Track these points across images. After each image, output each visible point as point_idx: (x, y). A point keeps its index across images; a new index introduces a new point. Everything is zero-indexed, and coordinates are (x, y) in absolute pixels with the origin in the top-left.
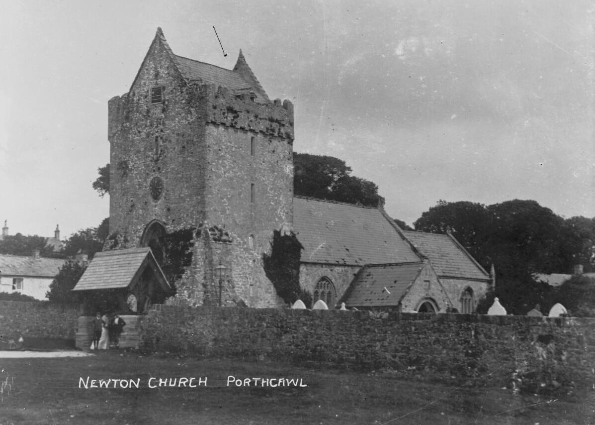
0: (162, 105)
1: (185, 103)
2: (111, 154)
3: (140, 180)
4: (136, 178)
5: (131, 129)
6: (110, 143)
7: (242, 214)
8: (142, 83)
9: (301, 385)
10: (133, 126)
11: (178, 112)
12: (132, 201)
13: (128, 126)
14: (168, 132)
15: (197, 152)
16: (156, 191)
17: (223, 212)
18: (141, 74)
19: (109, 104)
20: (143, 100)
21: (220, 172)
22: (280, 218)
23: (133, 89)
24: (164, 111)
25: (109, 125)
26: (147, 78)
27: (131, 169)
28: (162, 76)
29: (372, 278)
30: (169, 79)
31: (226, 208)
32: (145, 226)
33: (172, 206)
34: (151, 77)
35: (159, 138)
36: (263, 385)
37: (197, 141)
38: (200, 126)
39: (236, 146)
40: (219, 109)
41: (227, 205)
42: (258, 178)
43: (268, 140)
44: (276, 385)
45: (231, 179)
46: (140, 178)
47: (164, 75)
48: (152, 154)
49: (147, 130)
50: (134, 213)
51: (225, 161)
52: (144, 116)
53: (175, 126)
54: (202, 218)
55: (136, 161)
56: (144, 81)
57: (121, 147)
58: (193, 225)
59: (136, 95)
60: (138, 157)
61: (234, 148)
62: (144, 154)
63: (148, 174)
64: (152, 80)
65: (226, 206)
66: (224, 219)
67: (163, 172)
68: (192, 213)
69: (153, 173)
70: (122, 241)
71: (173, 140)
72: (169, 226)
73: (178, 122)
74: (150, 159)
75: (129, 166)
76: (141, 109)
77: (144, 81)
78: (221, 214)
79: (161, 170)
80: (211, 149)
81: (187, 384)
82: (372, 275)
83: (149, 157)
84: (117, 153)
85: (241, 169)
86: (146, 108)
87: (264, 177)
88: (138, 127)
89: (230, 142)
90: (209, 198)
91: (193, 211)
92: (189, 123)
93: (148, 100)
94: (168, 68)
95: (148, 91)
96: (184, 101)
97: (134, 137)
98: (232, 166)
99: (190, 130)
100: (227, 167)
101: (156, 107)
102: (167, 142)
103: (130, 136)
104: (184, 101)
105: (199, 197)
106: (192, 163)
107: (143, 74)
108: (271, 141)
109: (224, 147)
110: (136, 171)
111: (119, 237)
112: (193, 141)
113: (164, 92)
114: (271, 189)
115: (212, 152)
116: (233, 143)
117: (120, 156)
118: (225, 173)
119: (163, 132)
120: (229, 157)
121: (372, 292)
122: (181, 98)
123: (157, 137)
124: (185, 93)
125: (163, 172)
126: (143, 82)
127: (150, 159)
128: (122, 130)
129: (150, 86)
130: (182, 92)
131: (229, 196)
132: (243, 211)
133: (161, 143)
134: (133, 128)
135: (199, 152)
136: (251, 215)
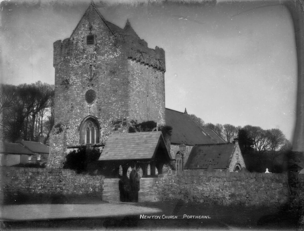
0: (95, 46)
1: (112, 45)
2: (56, 75)
3: (78, 92)
4: (75, 90)
5: (71, 60)
6: (55, 69)
7: (143, 113)
8: (79, 33)
9: (209, 218)
10: (72, 58)
11: (106, 51)
12: (72, 104)
13: (69, 58)
14: (99, 62)
15: (121, 75)
16: (90, 97)
17: (136, 112)
18: (78, 27)
19: (54, 45)
20: (80, 43)
21: (134, 88)
22: (160, 117)
23: (73, 36)
24: (96, 50)
25: (54, 58)
26: (83, 30)
27: (71, 85)
28: (95, 29)
29: (203, 152)
30: (99, 31)
31: (137, 109)
32: (82, 120)
33: (103, 107)
34: (86, 29)
35: (93, 66)
36: (140, 218)
37: (121, 68)
38: (124, 59)
39: (141, 73)
40: (134, 50)
41: (137, 107)
42: (150, 92)
43: (154, 70)
44: (200, 218)
45: (139, 92)
46: (78, 90)
47: (96, 28)
48: (87, 76)
49: (83, 61)
50: (73, 111)
51: (136, 82)
52: (81, 53)
53: (104, 59)
54: (126, 115)
55: (74, 79)
56: (81, 32)
57: (64, 71)
58: (119, 119)
59: (75, 40)
60: (76, 77)
61: (140, 74)
62: (81, 76)
63: (84, 88)
64: (87, 31)
65: (137, 108)
66: (136, 117)
67: (96, 86)
68: (117, 112)
69: (88, 87)
70: (65, 129)
71: (103, 68)
72: (101, 120)
73: (107, 57)
74: (85, 78)
75: (70, 82)
76: (79, 48)
77: (81, 32)
78: (135, 113)
79: (94, 86)
80: (130, 74)
81: (172, 217)
82: (202, 151)
83: (85, 77)
84: (61, 74)
85: (143, 87)
86: (83, 48)
87: (153, 92)
88: (77, 60)
89: (138, 70)
90: (129, 103)
91: (118, 111)
92: (115, 57)
93: (84, 43)
94: (99, 24)
95: (84, 38)
96: (111, 44)
97: (74, 65)
98: (139, 84)
99: (116, 62)
100: (137, 85)
101: (90, 47)
102: (99, 69)
103: (71, 64)
104: (111, 44)
105: (123, 103)
106: (117, 82)
107: (81, 27)
108: (155, 72)
109: (135, 73)
110: (75, 86)
111: (62, 126)
112: (118, 68)
113: (96, 39)
114: (156, 99)
115: (130, 75)
116: (139, 71)
117: (63, 76)
118: (136, 88)
119: (95, 62)
120: (138, 79)
121: (206, 160)
122: (109, 42)
123: (91, 65)
124: (112, 39)
125: (96, 86)
126: (80, 32)
127: (85, 78)
128: (64, 60)
129: (86, 35)
130: (109, 39)
131: (138, 103)
132: (144, 112)
133: (94, 69)
134: (73, 60)
135: (122, 75)
136: (147, 115)
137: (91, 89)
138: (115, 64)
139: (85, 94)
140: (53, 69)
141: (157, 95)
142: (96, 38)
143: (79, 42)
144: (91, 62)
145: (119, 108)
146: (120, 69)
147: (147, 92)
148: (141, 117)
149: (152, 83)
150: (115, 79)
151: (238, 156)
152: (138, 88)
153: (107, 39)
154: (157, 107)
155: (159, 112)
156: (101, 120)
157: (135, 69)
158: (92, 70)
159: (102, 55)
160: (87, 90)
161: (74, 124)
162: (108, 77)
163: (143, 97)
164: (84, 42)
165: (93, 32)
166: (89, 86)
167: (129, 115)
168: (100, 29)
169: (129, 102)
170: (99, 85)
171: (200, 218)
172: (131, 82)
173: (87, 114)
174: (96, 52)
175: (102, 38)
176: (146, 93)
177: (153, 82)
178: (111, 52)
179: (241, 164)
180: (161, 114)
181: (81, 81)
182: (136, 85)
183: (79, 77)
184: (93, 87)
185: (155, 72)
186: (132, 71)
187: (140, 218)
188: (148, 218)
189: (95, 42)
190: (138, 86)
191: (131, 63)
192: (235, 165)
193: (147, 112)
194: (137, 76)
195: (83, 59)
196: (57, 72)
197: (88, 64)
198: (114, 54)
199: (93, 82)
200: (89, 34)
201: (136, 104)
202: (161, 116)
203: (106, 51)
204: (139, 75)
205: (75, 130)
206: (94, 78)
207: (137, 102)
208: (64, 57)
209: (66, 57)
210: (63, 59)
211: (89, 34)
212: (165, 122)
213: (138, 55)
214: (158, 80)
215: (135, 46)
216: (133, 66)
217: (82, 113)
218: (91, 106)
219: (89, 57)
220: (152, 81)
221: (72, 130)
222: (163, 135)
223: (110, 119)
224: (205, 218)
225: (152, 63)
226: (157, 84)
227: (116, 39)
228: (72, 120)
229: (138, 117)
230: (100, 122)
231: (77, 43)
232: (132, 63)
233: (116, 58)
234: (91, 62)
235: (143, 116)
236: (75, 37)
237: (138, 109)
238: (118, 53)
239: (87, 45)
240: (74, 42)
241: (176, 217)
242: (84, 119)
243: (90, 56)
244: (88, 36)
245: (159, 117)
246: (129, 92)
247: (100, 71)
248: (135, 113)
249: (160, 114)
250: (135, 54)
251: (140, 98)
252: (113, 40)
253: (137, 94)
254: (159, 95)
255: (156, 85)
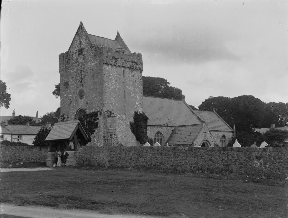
2: (61, 79)
5: (69, 67)
8: (74, 47)
12: (70, 100)
17: (112, 104)
20: (74, 54)
21: (110, 86)
22: (137, 106)
23: (70, 49)
24: (84, 59)
26: (76, 44)
31: (113, 102)
34: (78, 44)
35: (82, 71)
45: (115, 89)
48: (79, 78)
51: (112, 81)
55: (72, 81)
64: (78, 45)
69: (80, 87)
70: (66, 118)
76: (74, 58)
79: (83, 85)
83: (78, 80)
87: (129, 88)
89: (114, 73)
90: (105, 98)
92: (95, 64)
95: (77, 50)
96: (93, 55)
97: (71, 71)
98: (115, 83)
104: (93, 55)
108: (132, 72)
109: (111, 75)
113: (84, 51)
118: (112, 86)
119: (84, 68)
122: (92, 53)
123: (81, 71)
126: (74, 46)
127: (78, 80)
130: (92, 51)
131: (114, 97)
133: (83, 73)
134: (70, 67)
136: (124, 105)
137: (81, 88)
139: (78, 92)
140: (59, 75)
141: (134, 90)
145: (99, 101)
147: (123, 88)
148: (118, 107)
149: (129, 81)
150: (96, 80)
152: (115, 86)
155: (136, 102)
157: (111, 72)
159: (88, 63)
160: (79, 89)
162: (91, 79)
165: (82, 46)
166: (80, 86)
167: (105, 106)
173: (80, 107)
175: (87, 50)
176: (123, 89)
178: (93, 61)
180: (138, 104)
181: (76, 82)
184: (83, 87)
185: (132, 72)
186: (108, 73)
189: (83, 53)
191: (107, 68)
194: (113, 77)
195: (76, 66)
196: (61, 77)
198: (95, 62)
199: (83, 83)
201: (112, 98)
202: (139, 105)
204: (116, 76)
205: (73, 118)
206: (83, 80)
214: (135, 77)
217: (76, 106)
218: (82, 101)
219: (80, 65)
220: (128, 79)
221: (71, 119)
223: (93, 110)
226: (134, 81)
227: (96, 51)
231: (73, 54)
232: (105, 67)
236: (71, 51)
237: (114, 101)
238: (97, 61)
239: (79, 55)
242: (78, 110)
244: (79, 49)
245: (136, 107)
251: (116, 93)
252: (94, 51)
255: (133, 82)
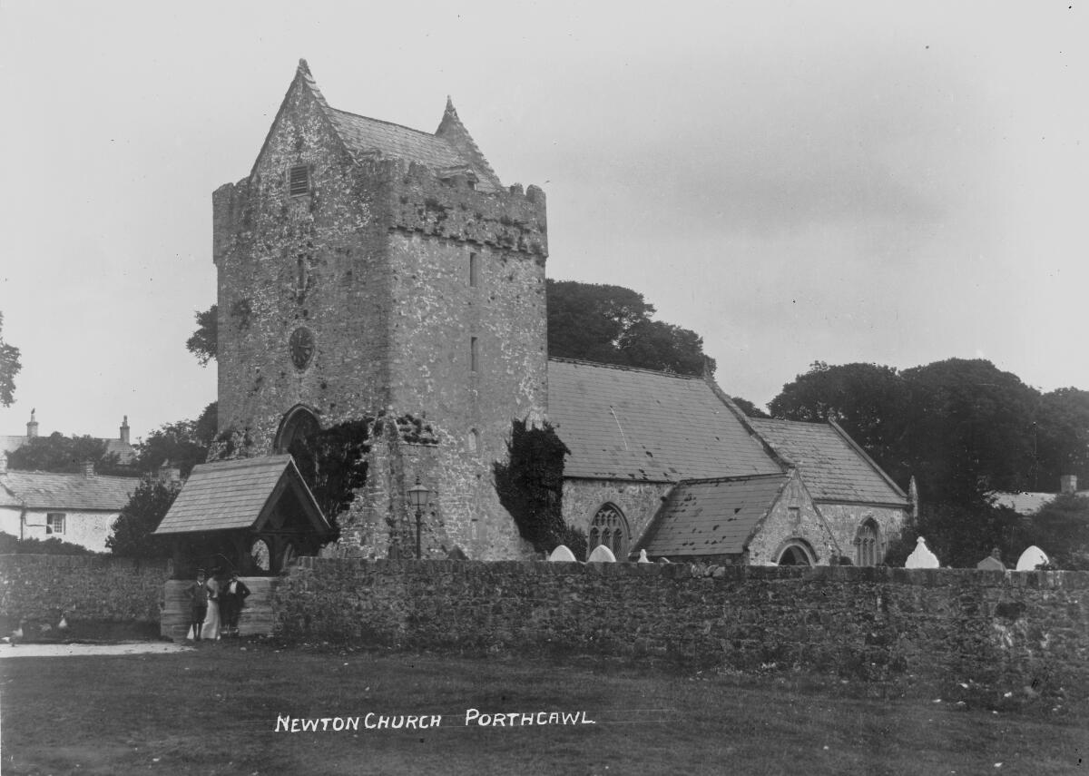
0: (310, 199)
1: (350, 193)
4: (265, 330)
5: (255, 242)
8: (273, 161)
9: (584, 721)
10: (257, 236)
12: (258, 371)
14: (321, 246)
16: (301, 352)
17: (422, 389)
21: (415, 317)
22: (525, 399)
24: (312, 208)
27: (257, 315)
31: (427, 381)
33: (331, 379)
34: (289, 149)
35: (305, 258)
43: (499, 258)
44: (545, 722)
45: (435, 329)
49: (282, 244)
50: (262, 392)
51: (424, 298)
60: (267, 292)
63: (285, 323)
64: (290, 153)
66: (424, 403)
67: (314, 318)
69: (296, 321)
70: (240, 445)
72: (325, 416)
78: (419, 392)
79: (309, 316)
80: (399, 277)
87: (494, 325)
89: (433, 264)
93: (283, 190)
94: (319, 132)
95: (283, 174)
96: (348, 191)
97: (261, 257)
100: (428, 308)
101: (298, 202)
104: (348, 191)
105: (378, 363)
107: (275, 144)
108: (505, 261)
109: (421, 272)
110: (264, 317)
112: (365, 261)
114: (508, 347)
117: (235, 290)
118: (424, 318)
119: (312, 247)
120: (432, 290)
123: (301, 256)
130: (344, 175)
131: (432, 361)
133: (308, 266)
134: (258, 241)
135: (377, 281)
136: (472, 395)
138: (359, 251)
142: (312, 173)
143: (271, 188)
144: (301, 247)
146: (371, 264)
147: (469, 326)
151: (798, 514)
152: (434, 317)
153: (338, 177)
154: (510, 369)
155: (521, 385)
156: (325, 416)
158: (303, 270)
161: (263, 429)
163: (454, 342)
164: (285, 188)
166: (297, 317)
168: (322, 145)
169: (397, 361)
170: (321, 314)
171: (545, 722)
172: (404, 300)
174: (314, 216)
177: (497, 293)
179: (812, 542)
180: (527, 390)
181: (279, 302)
182: (423, 308)
183: (274, 291)
184: (308, 319)
185: (505, 261)
187: (358, 719)
188: (305, 728)
190: (431, 310)
192: (782, 545)
193: (472, 387)
195: (281, 237)
197: (293, 251)
200: (296, 164)
203: (337, 213)
205: (265, 447)
207: (428, 359)
208: (239, 233)
209: (243, 235)
210: (234, 239)
211: (296, 164)
212: (331, 425)
213: (430, 218)
215: (417, 193)
216: (412, 252)
218: (302, 375)
219: (297, 231)
221: (260, 448)
222: (296, 464)
224: (565, 721)
225: (490, 235)
228: (260, 417)
229: (430, 404)
230: (324, 423)
233: (362, 232)
234: (301, 247)
235: (455, 399)
236: (263, 174)
237: (432, 380)
240: (261, 188)
241: (436, 721)
243: (299, 228)
244: (293, 169)
245: (518, 401)
246: (395, 331)
247: (322, 273)
248: (419, 392)
249: (523, 391)
250: (417, 215)
253: (426, 336)
254: (519, 332)
